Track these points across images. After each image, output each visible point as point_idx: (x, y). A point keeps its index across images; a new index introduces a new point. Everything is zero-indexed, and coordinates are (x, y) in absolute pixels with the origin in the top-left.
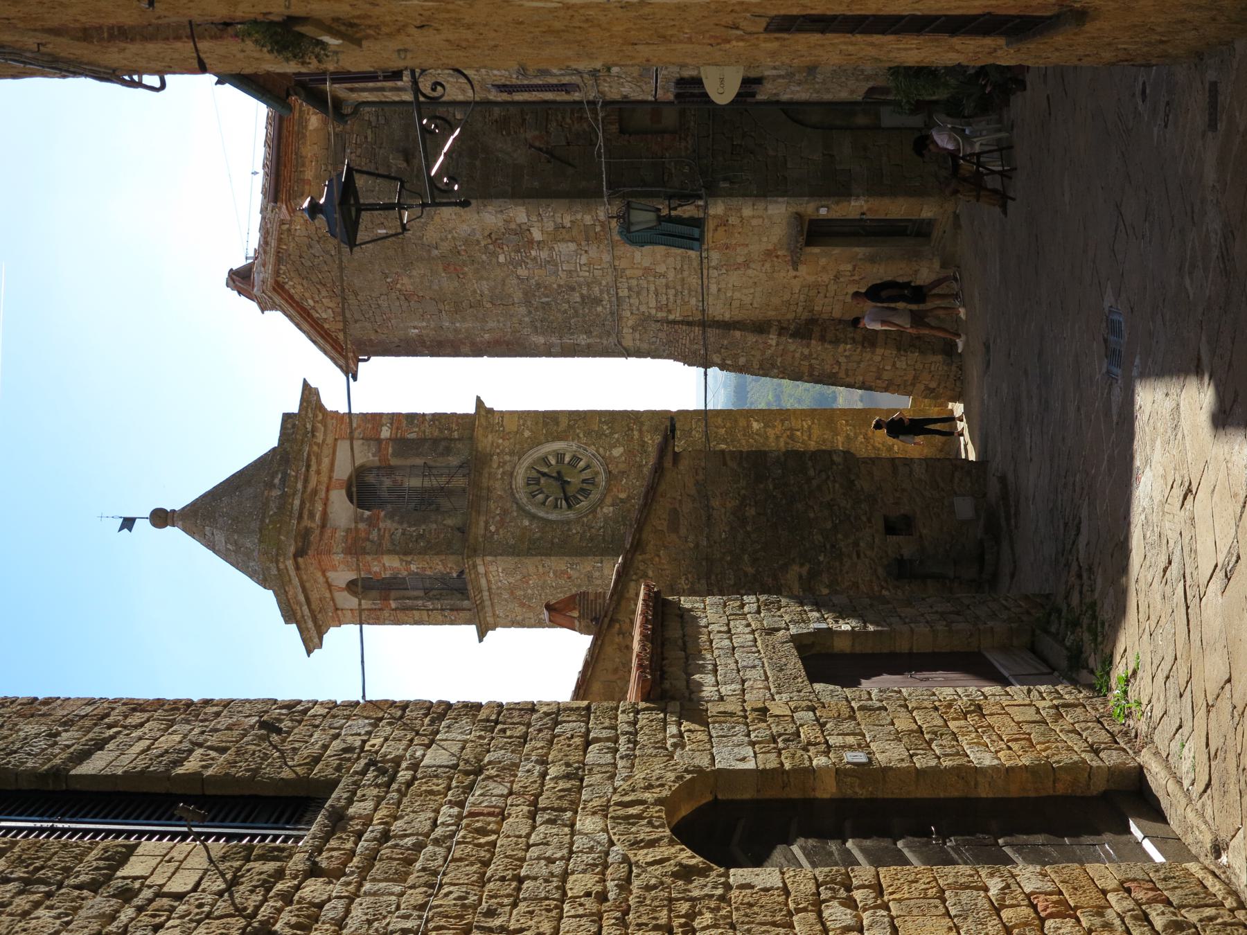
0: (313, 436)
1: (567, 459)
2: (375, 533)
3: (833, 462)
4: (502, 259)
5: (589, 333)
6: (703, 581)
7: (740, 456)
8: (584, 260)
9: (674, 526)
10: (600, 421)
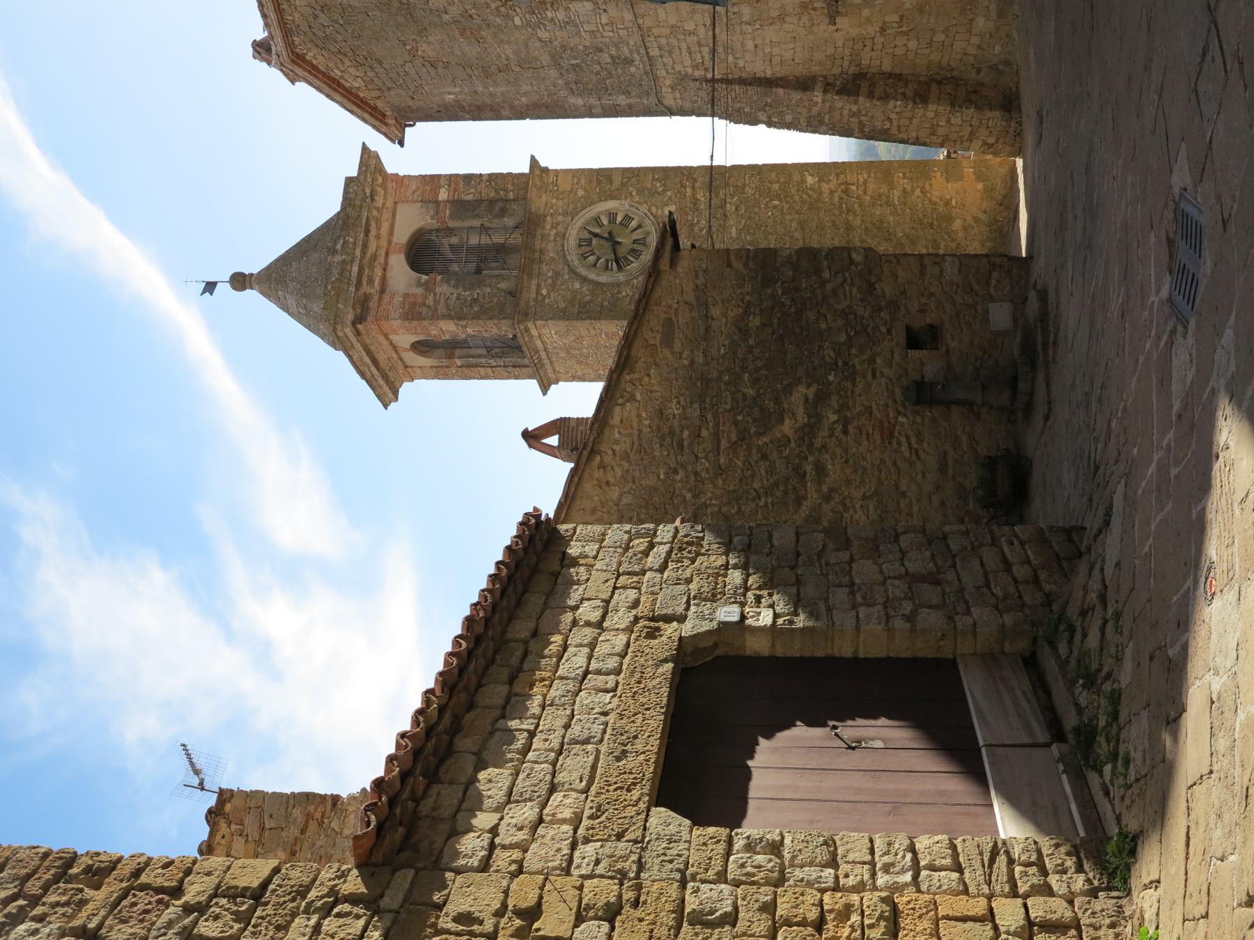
0: (373, 200)
1: (619, 219)
2: (431, 298)
3: (852, 262)
4: (517, 21)
5: (627, 93)
6: (696, 405)
7: (745, 255)
8: (604, 20)
9: (668, 340)
10: (653, 178)
